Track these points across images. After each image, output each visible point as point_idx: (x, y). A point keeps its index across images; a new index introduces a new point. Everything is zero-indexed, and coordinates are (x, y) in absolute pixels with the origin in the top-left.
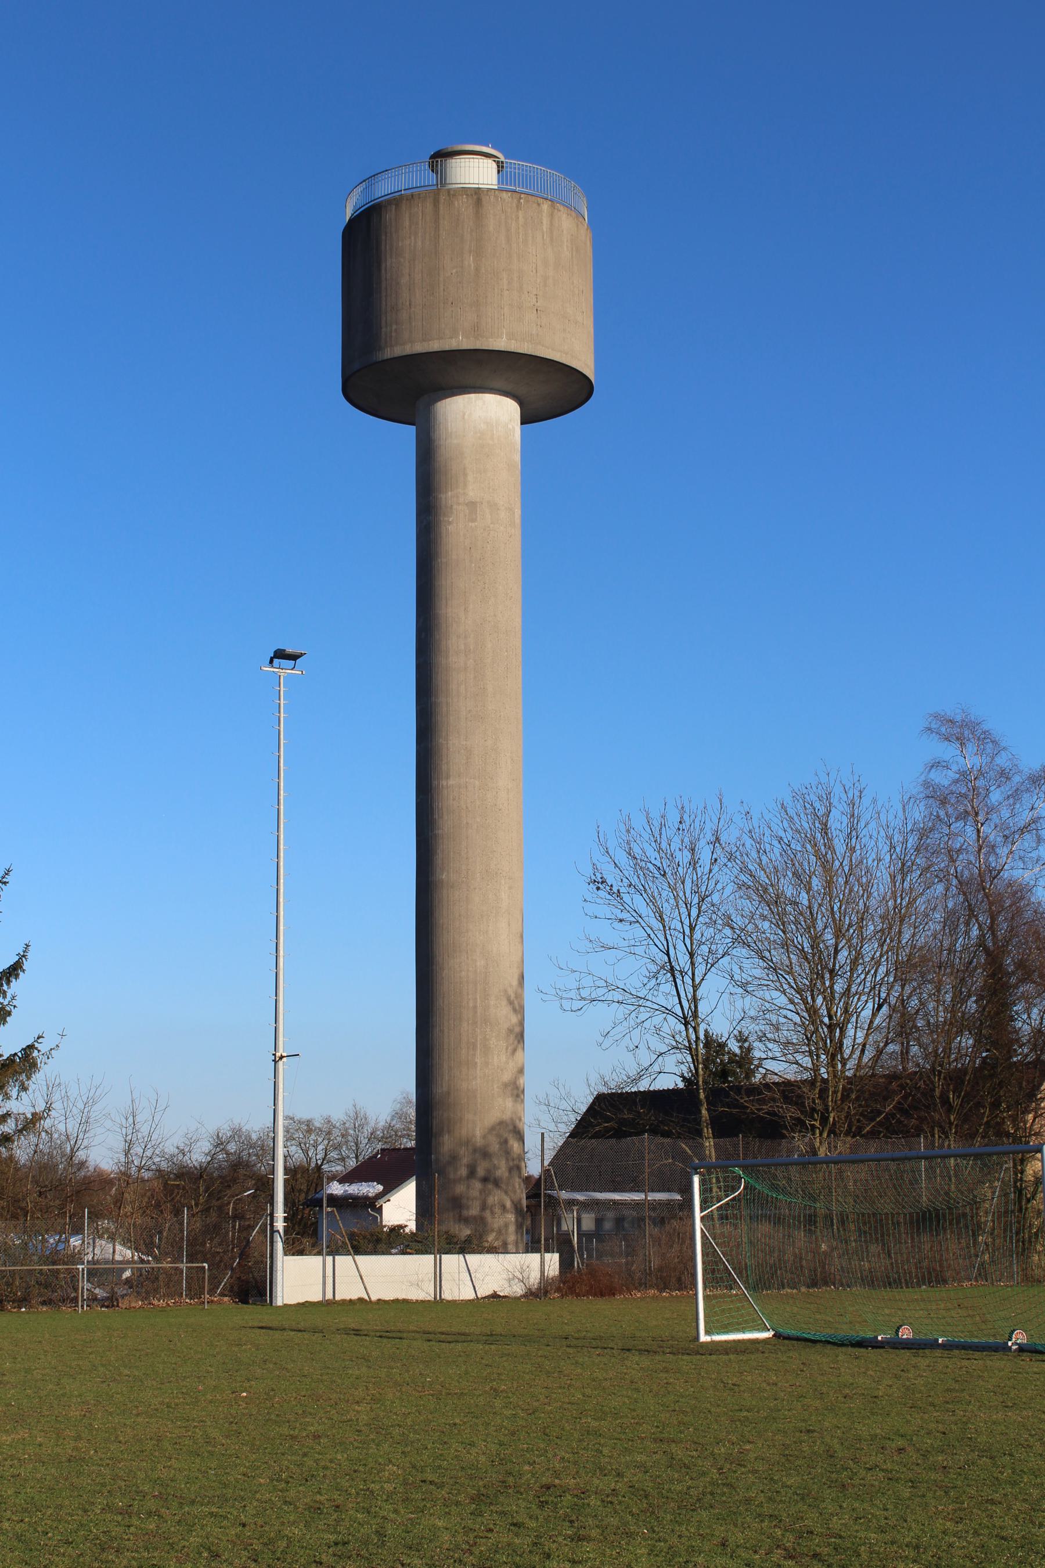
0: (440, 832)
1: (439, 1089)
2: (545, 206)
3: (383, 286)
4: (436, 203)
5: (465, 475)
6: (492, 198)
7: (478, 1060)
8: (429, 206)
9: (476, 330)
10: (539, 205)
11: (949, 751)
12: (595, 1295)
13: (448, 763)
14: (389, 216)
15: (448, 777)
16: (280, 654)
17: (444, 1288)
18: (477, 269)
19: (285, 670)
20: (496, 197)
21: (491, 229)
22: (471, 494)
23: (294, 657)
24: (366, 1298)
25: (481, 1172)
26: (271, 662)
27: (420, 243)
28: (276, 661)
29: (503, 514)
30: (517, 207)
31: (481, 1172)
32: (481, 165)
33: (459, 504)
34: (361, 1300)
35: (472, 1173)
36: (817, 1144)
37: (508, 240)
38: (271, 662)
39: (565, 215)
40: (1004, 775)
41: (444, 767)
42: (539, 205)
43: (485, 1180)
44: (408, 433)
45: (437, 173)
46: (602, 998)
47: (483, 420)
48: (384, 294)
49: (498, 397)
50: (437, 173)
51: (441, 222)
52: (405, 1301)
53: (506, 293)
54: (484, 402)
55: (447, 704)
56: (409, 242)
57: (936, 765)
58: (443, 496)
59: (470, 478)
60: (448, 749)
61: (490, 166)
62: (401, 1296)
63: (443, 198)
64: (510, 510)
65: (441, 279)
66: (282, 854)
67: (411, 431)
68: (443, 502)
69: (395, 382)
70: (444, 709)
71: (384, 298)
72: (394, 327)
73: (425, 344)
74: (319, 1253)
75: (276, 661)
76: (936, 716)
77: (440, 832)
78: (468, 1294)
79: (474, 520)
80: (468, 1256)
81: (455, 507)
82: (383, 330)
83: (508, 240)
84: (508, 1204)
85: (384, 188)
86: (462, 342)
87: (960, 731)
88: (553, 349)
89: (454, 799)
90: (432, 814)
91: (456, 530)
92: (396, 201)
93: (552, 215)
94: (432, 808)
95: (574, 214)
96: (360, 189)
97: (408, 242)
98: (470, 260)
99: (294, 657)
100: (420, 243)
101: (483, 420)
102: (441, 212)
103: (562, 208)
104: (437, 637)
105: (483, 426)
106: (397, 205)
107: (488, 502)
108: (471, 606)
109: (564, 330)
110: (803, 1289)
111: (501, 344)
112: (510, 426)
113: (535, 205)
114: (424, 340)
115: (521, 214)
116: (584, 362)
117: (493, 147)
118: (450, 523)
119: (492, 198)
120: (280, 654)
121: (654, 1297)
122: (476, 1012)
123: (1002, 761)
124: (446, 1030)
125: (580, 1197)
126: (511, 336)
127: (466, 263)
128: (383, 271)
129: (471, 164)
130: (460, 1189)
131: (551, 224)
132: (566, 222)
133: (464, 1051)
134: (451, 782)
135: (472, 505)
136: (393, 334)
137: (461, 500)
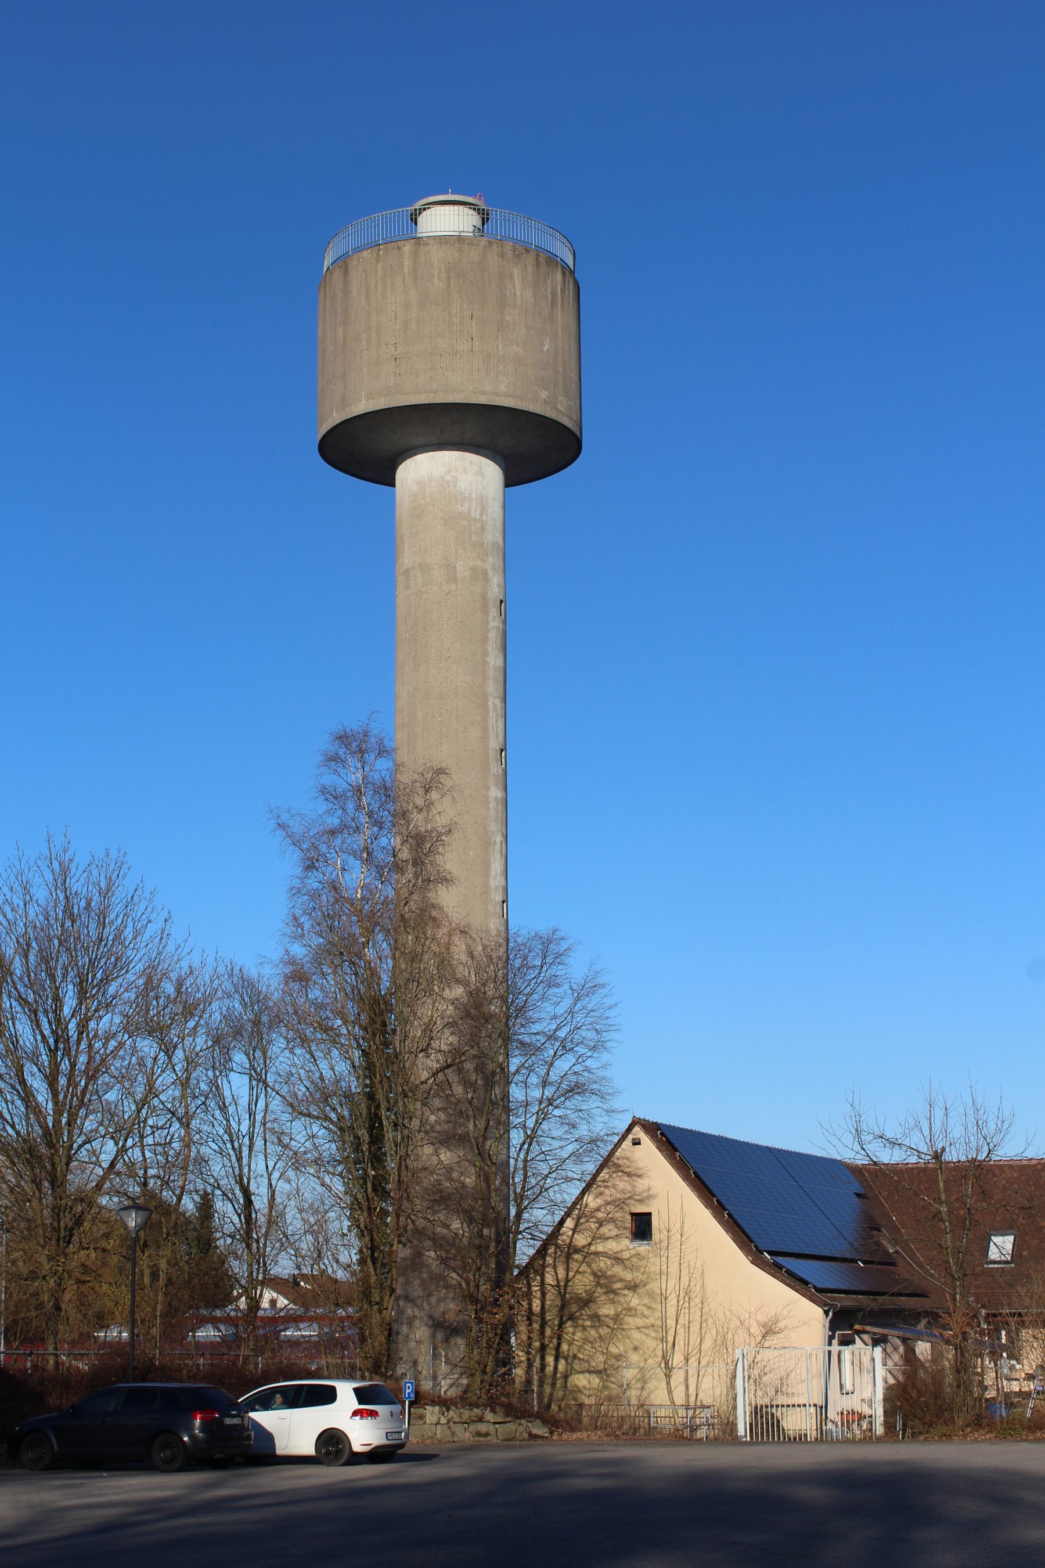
22: (406, 561)
32: (447, 212)
42: (399, 248)
112: (448, 478)
113: (396, 251)
117: (452, 193)
125: (184, 1385)
131: (415, 263)
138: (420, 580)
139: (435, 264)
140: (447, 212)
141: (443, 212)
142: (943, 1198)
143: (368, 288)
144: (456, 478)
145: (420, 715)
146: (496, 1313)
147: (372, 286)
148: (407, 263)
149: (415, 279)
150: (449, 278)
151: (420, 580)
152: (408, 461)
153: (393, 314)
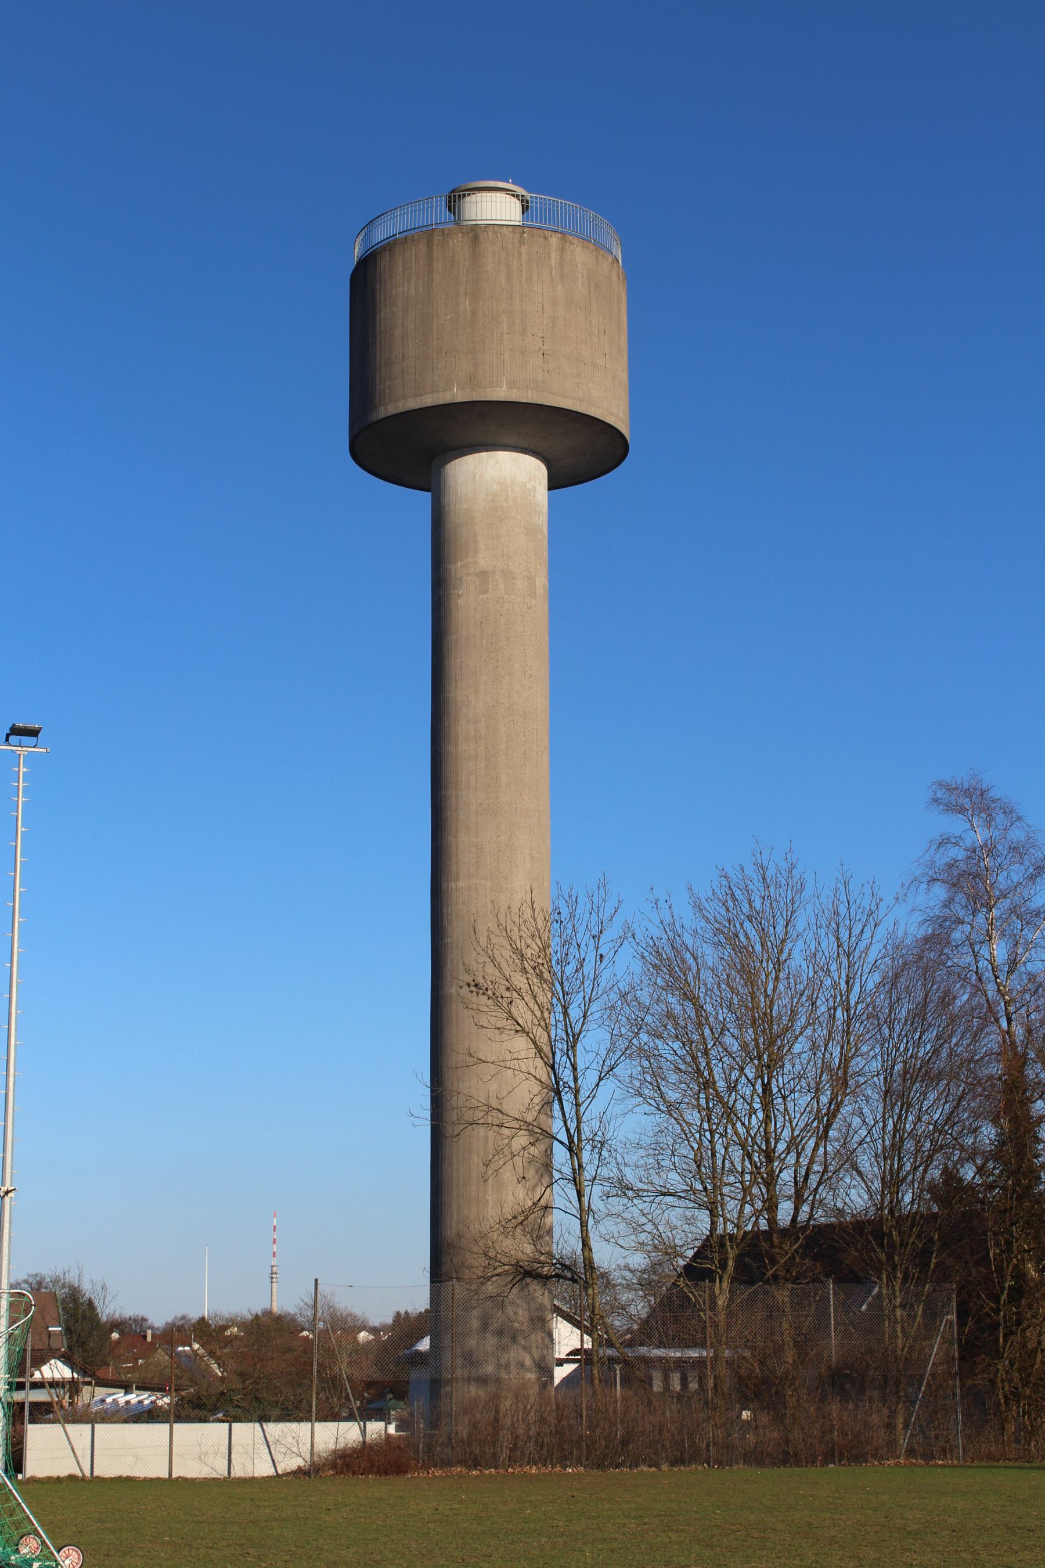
0: (449, 940)
1: (450, 1232)
2: (554, 240)
3: (378, 340)
4: (430, 244)
5: (476, 542)
6: (491, 234)
7: (489, 1198)
8: (423, 247)
9: (473, 380)
10: (546, 238)
11: (956, 825)
12: (378, 1473)
13: (457, 863)
14: (383, 262)
15: (457, 880)
16: (15, 731)
17: (234, 1462)
18: (474, 313)
19: (23, 748)
20: (495, 233)
21: (489, 268)
22: (482, 562)
23: (34, 733)
24: (80, 1475)
25: (495, 1325)
26: (7, 739)
27: (413, 290)
28: (11, 737)
29: (520, 584)
30: (520, 242)
31: (495, 1325)
32: (498, 200)
33: (469, 574)
34: (72, 1478)
35: (485, 1326)
36: (717, 1292)
37: (509, 278)
38: (7, 739)
39: (579, 249)
40: (1017, 850)
41: (454, 868)
42: (546, 238)
43: (500, 1333)
44: (425, 498)
45: (454, 214)
46: (481, 1122)
47: (502, 479)
48: (378, 348)
49: (514, 455)
50: (454, 214)
51: (435, 264)
52: (129, 1479)
53: (506, 337)
54: (497, 461)
55: (457, 796)
56: (402, 287)
57: (944, 842)
58: (452, 567)
59: (481, 545)
60: (457, 848)
61: (517, 205)
62: (125, 1474)
63: (437, 238)
64: (531, 580)
65: (435, 327)
66: (15, 959)
67: (428, 495)
68: (453, 574)
69: (407, 446)
70: (454, 803)
71: (378, 353)
72: (388, 383)
73: (418, 399)
74: (308, 1419)
75: (11, 737)
76: (940, 784)
77: (449, 940)
78: (263, 1469)
79: (486, 592)
80: (265, 1425)
81: (464, 578)
82: (378, 387)
83: (509, 278)
84: (528, 1361)
85: (381, 233)
86: (458, 395)
87: (971, 800)
88: (563, 396)
89: (463, 904)
90: (442, 922)
91: (467, 603)
92: (390, 246)
93: (562, 249)
94: (442, 913)
95: (591, 246)
96: (361, 237)
97: (401, 290)
98: (466, 305)
99: (34, 733)
100: (413, 290)
101: (502, 479)
102: (435, 254)
103: (575, 241)
104: (447, 723)
105: (495, 487)
106: (390, 250)
107: (502, 571)
108: (482, 687)
109: (579, 375)
110: (665, 1467)
111: (501, 393)
112: (529, 486)
113: (541, 240)
114: (416, 395)
115: (524, 249)
116: (611, 406)
117: (513, 183)
118: (460, 596)
119: (491, 234)
120: (15, 731)
121: (459, 1475)
122: (487, 1143)
123: (1017, 834)
124: (454, 1162)
125: (675, 1354)
126: (512, 385)
127: (462, 307)
128: (378, 324)
129: (484, 199)
130: (472, 1342)
131: (562, 258)
132: (581, 255)
133: (473, 1188)
134: (461, 884)
135: (484, 575)
136: (387, 391)
137: (471, 570)
138: (502, 586)
139: (579, 266)
140: (494, 199)
141: (503, 200)
142: (899, 1300)
143: (509, 268)
144: (534, 487)
145: (503, 730)
146: (1020, 1275)
147: (515, 268)
148: (554, 256)
149: (562, 276)
150: (589, 285)
151: (502, 586)
152: (484, 454)
153: (540, 306)
